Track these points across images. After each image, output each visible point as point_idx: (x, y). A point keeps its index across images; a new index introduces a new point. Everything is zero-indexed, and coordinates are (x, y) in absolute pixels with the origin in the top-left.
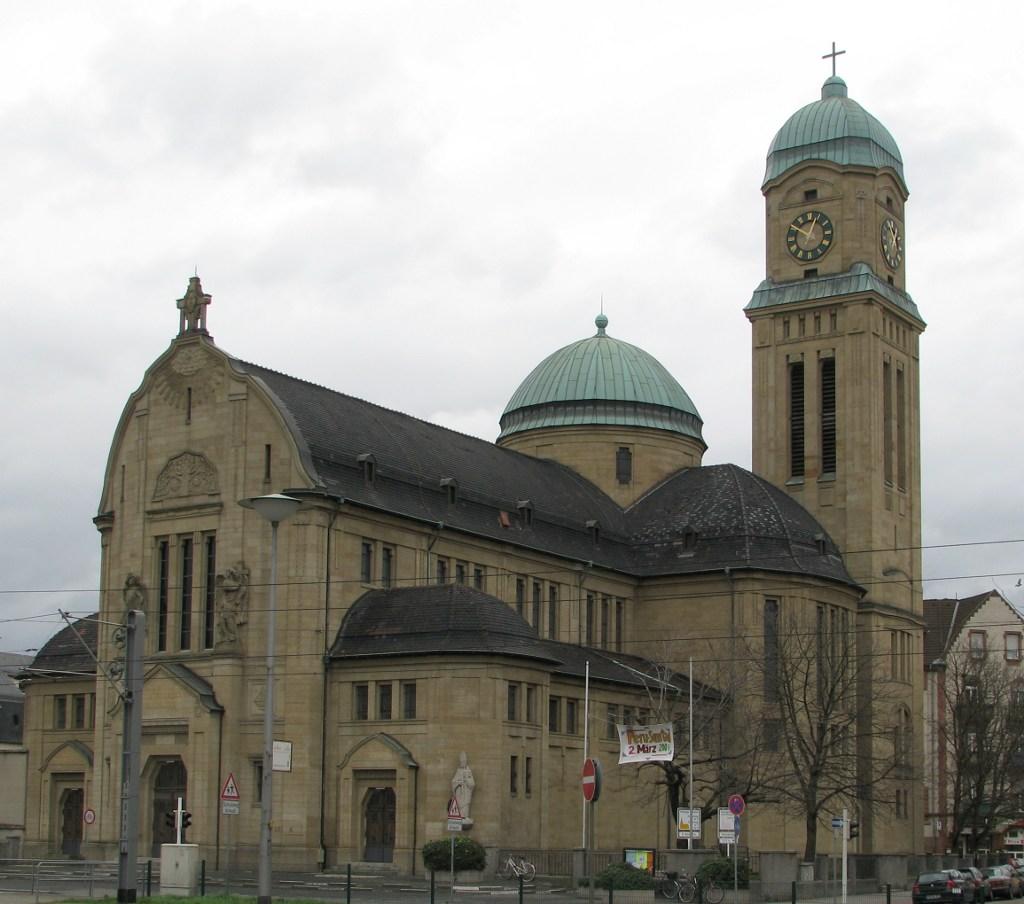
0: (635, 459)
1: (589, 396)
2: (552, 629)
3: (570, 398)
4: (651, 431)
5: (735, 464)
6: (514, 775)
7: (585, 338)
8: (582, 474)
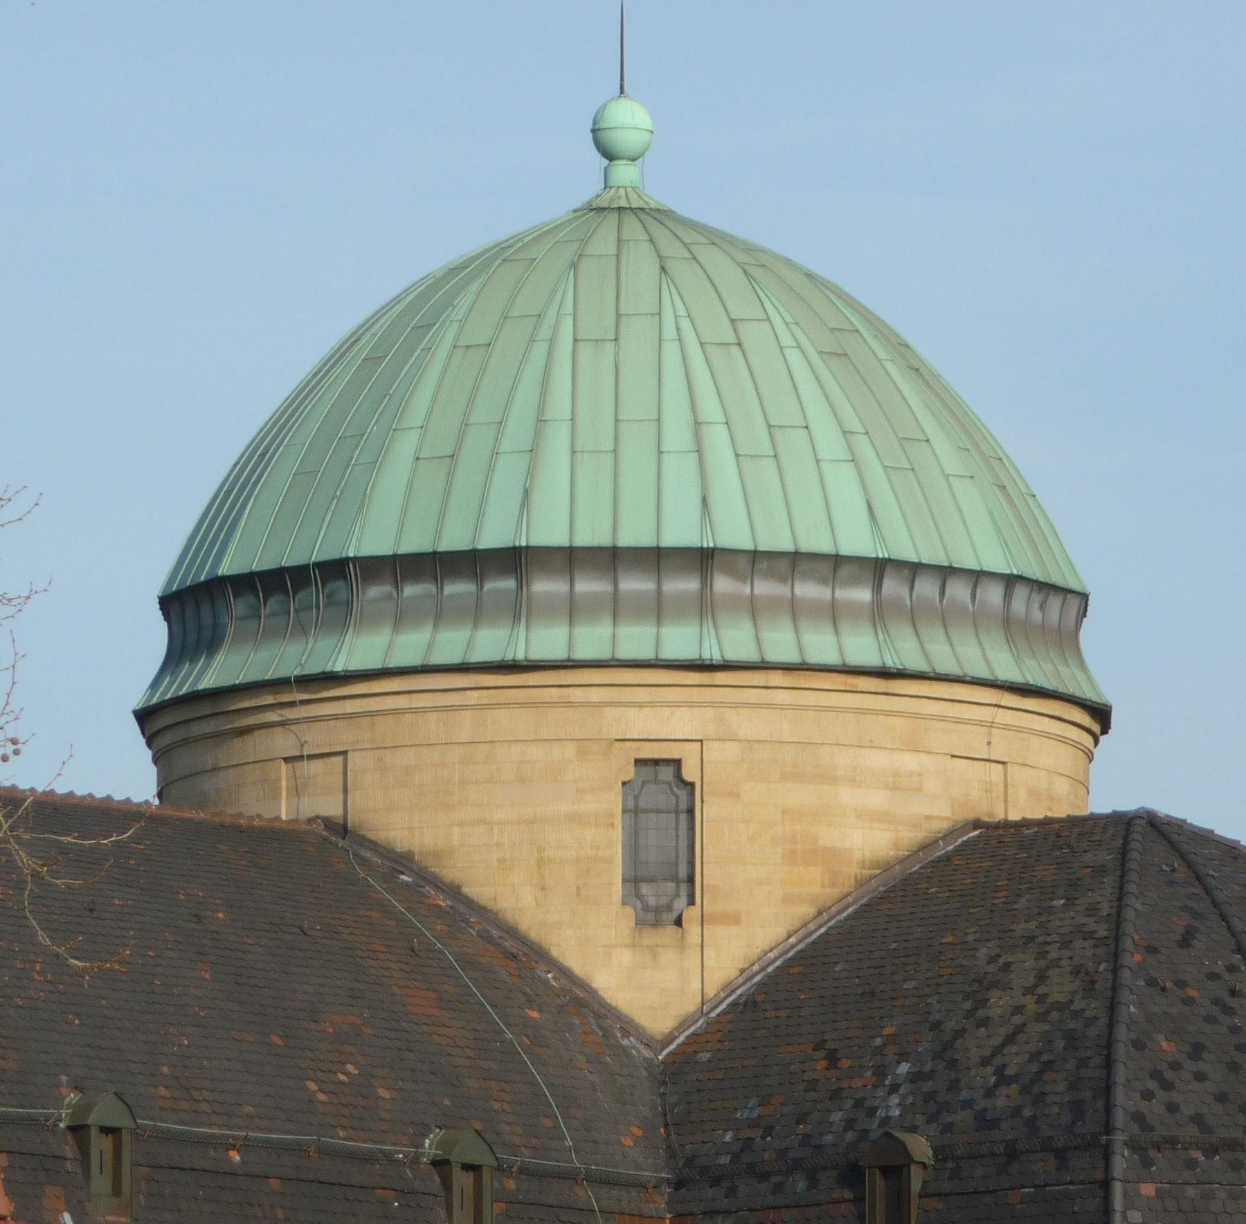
0: (710, 811)
1: (493, 537)
4: (777, 678)
5: (1168, 806)
8: (468, 890)
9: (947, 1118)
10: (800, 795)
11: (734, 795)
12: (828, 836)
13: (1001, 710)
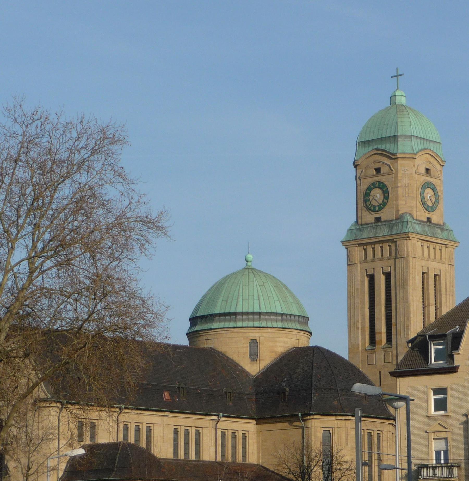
0: (260, 346)
2: (198, 453)
3: (222, 311)
7: (224, 275)
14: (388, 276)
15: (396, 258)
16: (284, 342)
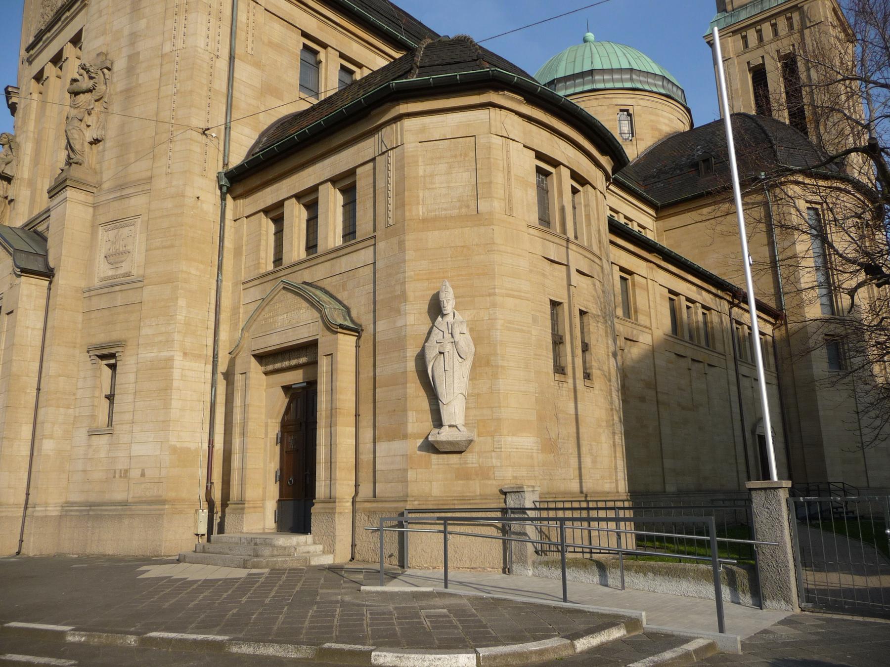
1: (587, 68)
6: (558, 341)
9: (73, 398)
10: (653, 118)
11: (640, 116)
12: (659, 126)
13: (372, 485)
14: (789, 65)
15: (803, 27)
16: (670, 119)
